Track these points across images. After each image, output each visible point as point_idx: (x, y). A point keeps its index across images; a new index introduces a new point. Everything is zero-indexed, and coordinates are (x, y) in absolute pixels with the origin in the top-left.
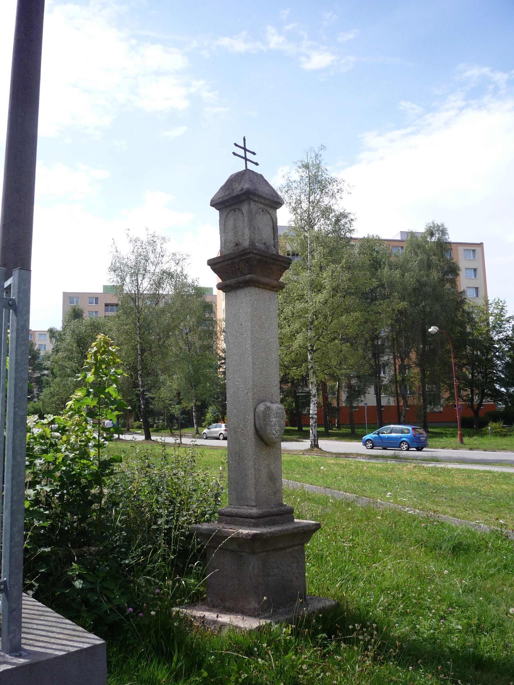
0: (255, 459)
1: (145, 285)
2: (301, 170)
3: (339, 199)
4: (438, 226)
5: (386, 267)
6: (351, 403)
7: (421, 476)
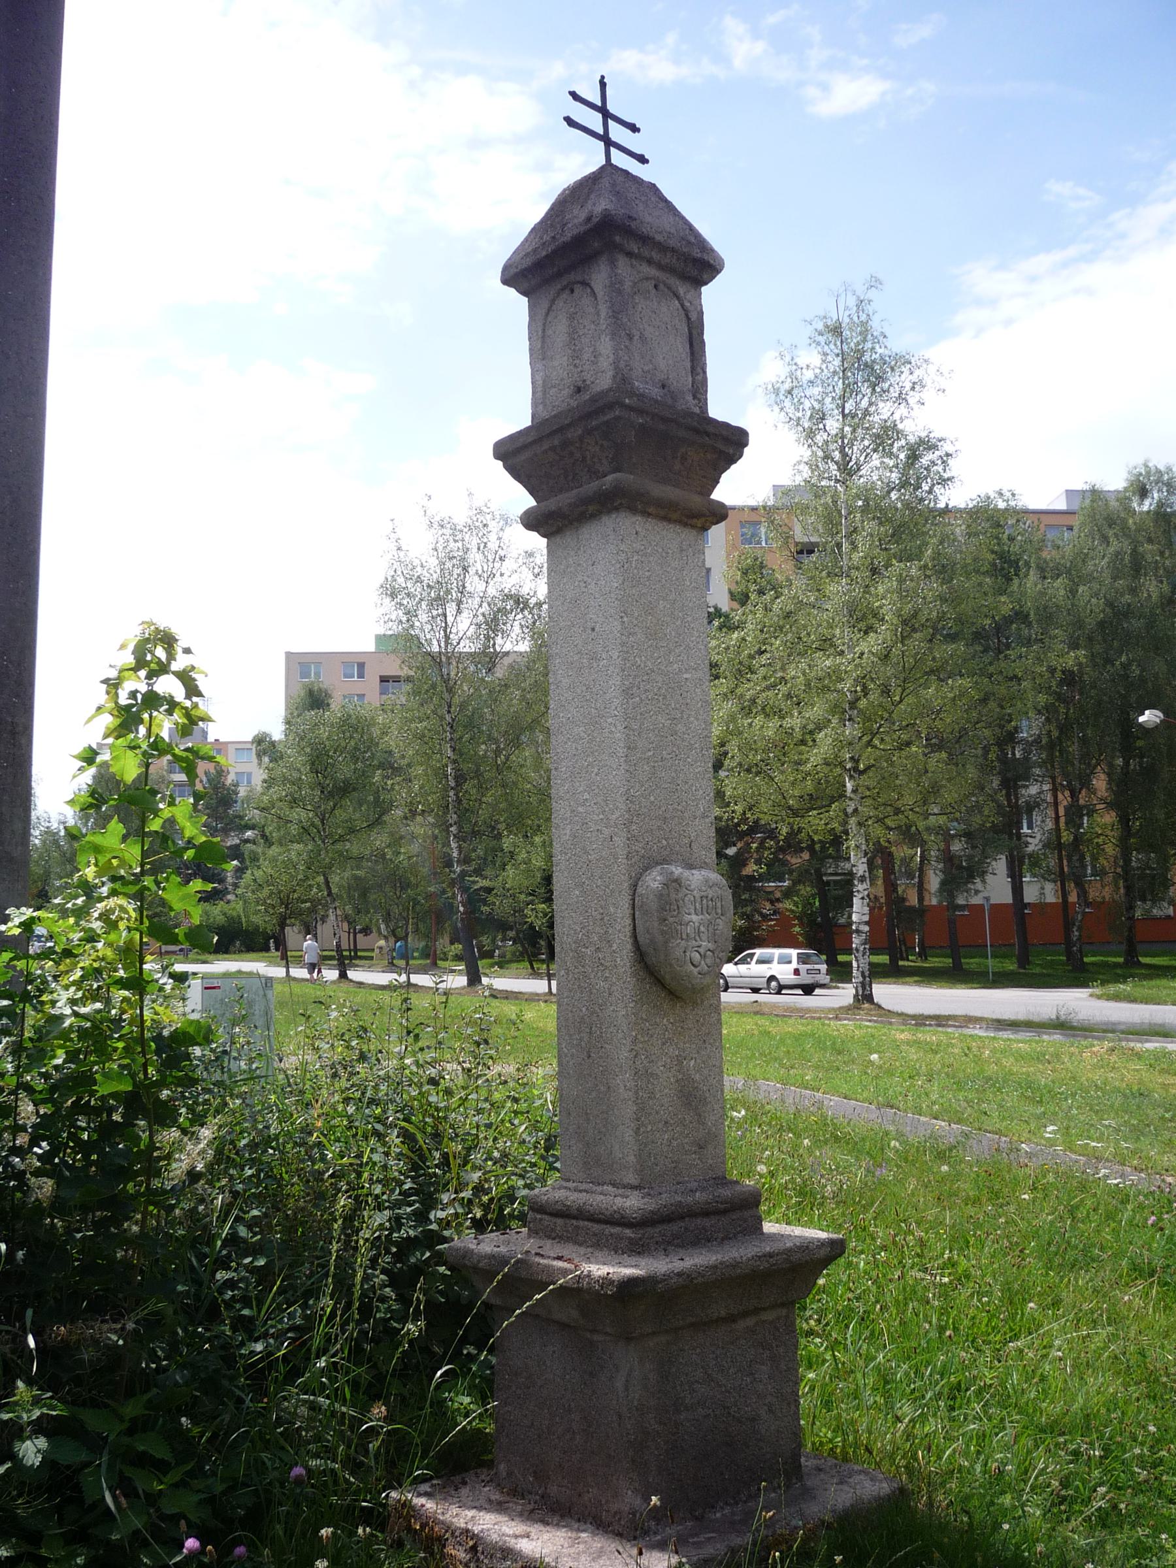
0: (635, 1041)
1: (464, 630)
2: (822, 339)
3: (916, 407)
4: (1159, 472)
5: (1031, 573)
6: (952, 896)
7: (1131, 1074)
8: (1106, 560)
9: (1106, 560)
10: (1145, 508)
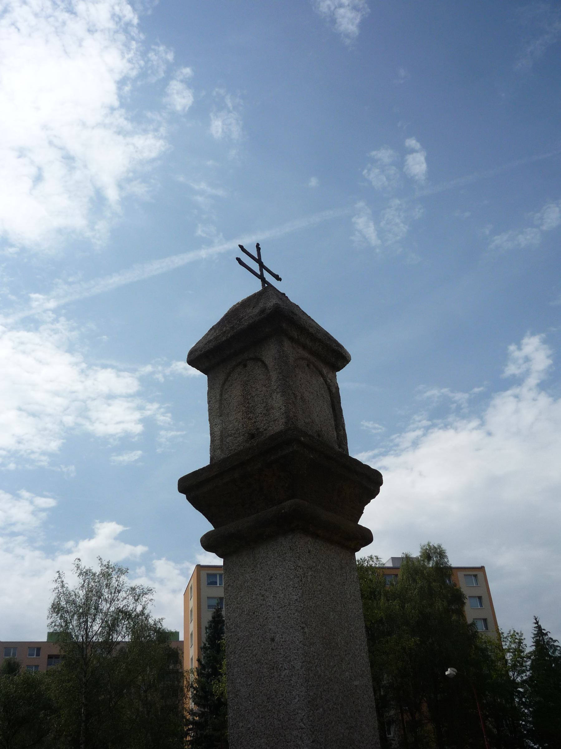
10: (431, 566)
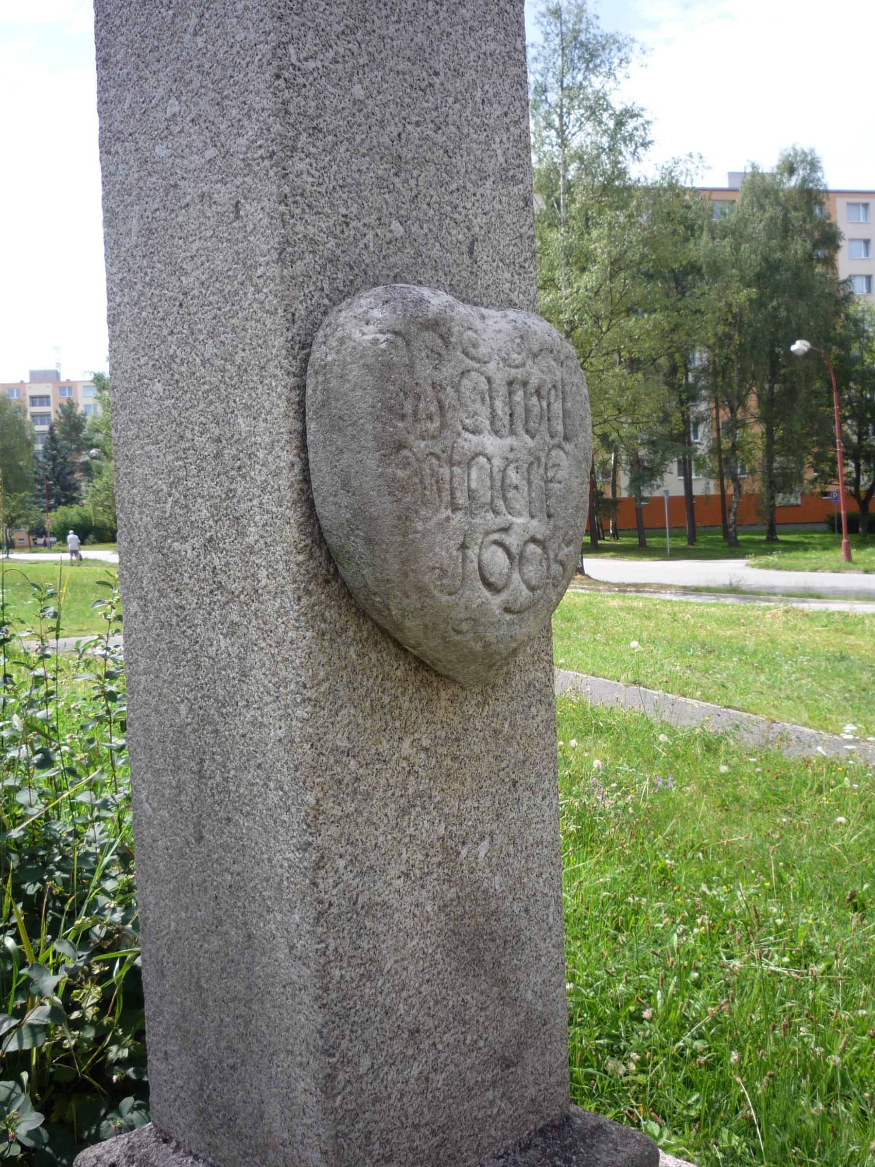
0: (315, 819)
2: (544, 21)
4: (804, 153)
8: (763, 223)
9: (763, 223)
